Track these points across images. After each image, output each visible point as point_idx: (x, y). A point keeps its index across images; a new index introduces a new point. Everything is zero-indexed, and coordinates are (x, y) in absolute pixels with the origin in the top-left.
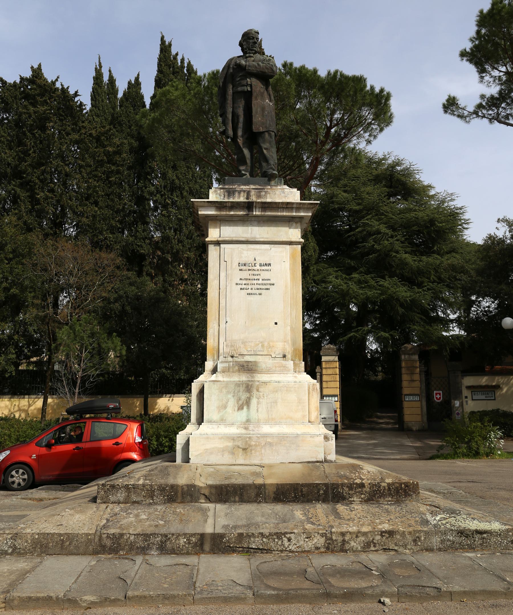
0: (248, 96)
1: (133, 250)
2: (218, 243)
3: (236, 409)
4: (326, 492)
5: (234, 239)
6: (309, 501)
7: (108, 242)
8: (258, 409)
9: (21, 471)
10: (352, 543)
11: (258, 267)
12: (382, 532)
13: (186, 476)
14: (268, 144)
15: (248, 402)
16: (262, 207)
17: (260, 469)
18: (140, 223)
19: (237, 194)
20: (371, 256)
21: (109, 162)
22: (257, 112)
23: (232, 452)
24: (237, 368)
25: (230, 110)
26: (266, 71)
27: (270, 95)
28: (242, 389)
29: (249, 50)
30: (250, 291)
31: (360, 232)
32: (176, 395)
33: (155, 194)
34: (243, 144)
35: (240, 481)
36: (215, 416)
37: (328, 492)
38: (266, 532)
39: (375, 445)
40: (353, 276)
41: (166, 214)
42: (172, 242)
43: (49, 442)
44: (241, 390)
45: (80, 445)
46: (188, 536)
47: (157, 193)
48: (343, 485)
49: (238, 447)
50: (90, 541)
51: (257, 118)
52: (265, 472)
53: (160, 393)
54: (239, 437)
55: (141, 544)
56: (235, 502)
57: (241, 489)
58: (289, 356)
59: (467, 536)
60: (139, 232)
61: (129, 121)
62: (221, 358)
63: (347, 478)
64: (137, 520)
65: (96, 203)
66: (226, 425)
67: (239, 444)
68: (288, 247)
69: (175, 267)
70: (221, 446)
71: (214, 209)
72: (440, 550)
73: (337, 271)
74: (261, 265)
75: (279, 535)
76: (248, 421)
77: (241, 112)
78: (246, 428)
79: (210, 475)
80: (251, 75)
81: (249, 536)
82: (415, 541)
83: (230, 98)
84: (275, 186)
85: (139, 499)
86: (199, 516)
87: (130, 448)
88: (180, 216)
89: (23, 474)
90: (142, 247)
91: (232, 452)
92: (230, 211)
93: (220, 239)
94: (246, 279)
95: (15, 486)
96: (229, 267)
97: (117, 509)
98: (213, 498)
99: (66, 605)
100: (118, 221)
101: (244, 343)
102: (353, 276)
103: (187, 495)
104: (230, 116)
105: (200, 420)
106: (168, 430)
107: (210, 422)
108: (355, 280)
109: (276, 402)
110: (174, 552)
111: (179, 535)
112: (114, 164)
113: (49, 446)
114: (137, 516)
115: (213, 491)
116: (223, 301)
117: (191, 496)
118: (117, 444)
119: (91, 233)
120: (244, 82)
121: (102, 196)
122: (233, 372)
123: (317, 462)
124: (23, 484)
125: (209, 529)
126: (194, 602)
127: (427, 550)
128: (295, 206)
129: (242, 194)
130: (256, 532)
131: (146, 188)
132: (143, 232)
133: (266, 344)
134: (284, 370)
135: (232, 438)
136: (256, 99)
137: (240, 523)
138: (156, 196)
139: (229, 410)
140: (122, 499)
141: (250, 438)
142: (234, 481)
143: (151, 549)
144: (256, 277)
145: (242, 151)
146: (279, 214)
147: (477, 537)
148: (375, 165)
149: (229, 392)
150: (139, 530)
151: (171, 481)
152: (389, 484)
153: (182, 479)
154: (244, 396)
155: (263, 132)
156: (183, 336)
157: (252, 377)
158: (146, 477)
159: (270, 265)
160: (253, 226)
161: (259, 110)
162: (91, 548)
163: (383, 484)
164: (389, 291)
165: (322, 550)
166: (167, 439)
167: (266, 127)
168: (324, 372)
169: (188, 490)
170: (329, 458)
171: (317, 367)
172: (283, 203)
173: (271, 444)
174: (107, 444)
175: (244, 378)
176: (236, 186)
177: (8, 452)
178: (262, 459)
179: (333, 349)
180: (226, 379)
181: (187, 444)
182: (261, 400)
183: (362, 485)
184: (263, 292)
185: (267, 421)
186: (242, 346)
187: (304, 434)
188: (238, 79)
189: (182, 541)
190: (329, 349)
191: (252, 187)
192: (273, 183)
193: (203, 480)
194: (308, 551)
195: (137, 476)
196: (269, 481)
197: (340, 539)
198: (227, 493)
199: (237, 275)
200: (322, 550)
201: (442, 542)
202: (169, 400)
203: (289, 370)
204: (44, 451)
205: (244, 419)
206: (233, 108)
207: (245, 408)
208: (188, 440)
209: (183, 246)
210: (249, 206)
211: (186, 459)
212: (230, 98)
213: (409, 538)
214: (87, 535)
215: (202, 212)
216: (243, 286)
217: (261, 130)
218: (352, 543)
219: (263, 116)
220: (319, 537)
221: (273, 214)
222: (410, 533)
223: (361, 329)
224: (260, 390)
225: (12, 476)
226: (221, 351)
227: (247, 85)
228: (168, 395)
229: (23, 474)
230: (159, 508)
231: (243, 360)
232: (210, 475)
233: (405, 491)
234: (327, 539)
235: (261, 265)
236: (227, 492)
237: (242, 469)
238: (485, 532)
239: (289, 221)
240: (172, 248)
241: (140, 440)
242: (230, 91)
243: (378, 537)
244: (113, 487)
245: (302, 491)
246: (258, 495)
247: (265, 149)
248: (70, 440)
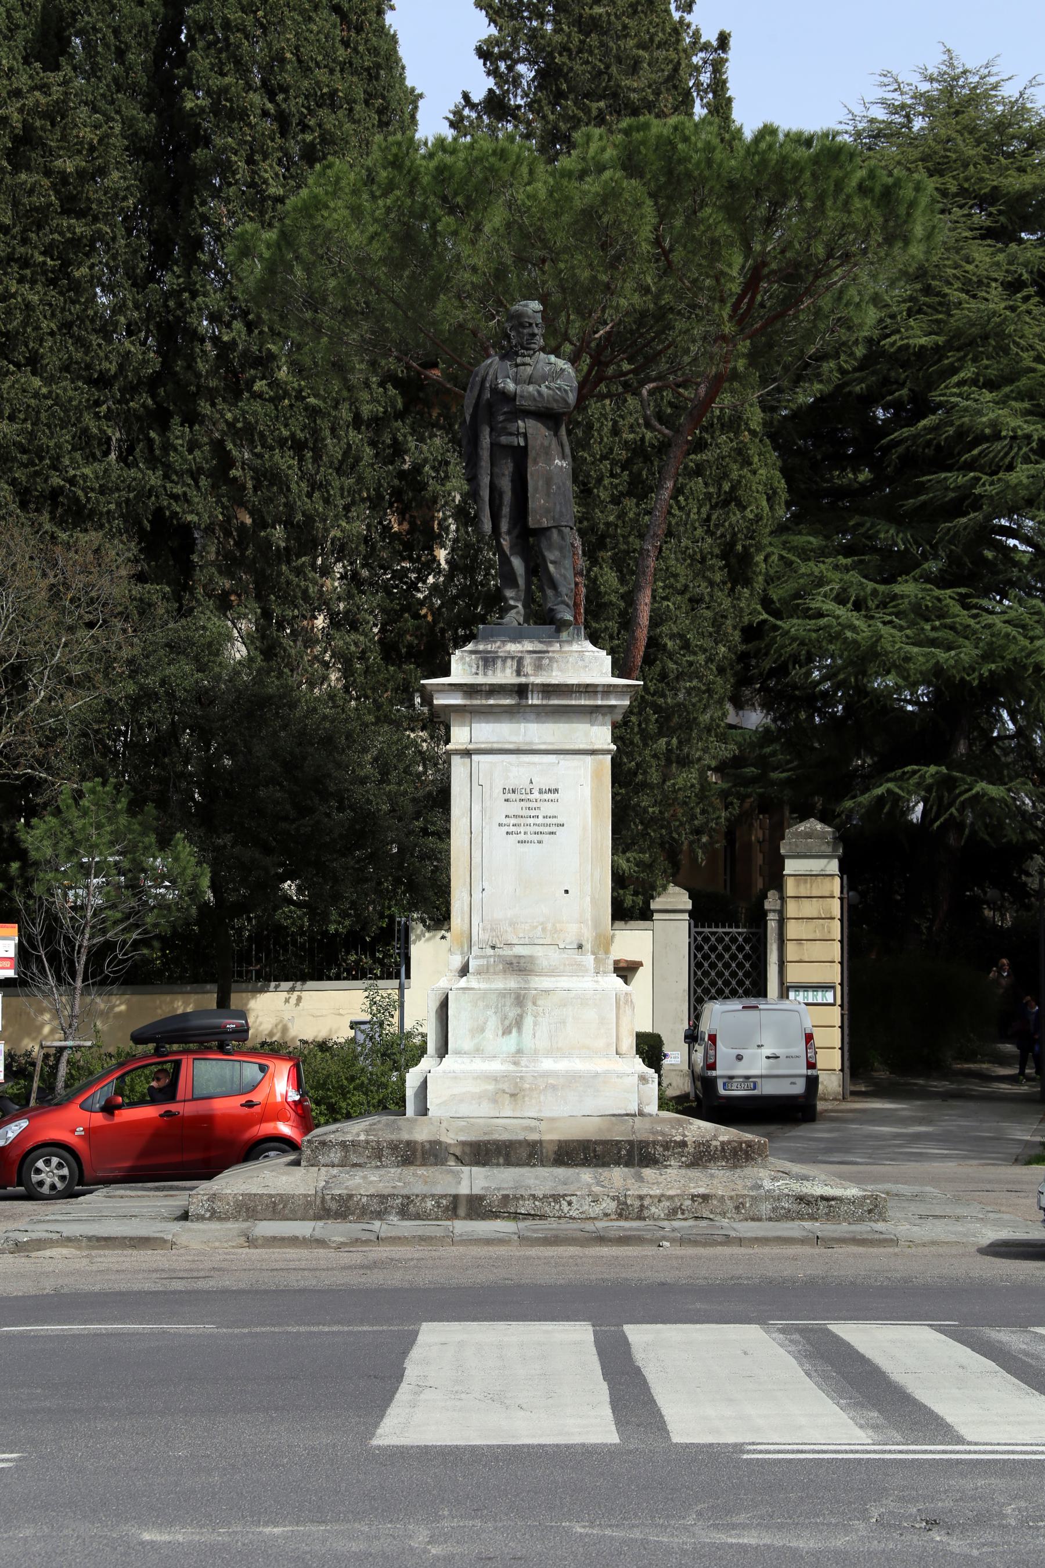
0: (520, 456)
1: (159, 510)
2: (467, 753)
3: (500, 1033)
4: (630, 1153)
5: (496, 746)
6: (605, 1165)
7: (80, 493)
8: (535, 1032)
9: (55, 1160)
10: (653, 1209)
11: (536, 795)
12: (693, 1196)
13: (426, 1131)
14: (557, 553)
15: (519, 1023)
16: (543, 692)
17: (533, 1123)
18: (177, 419)
19: (499, 663)
20: (964, 520)
21: (66, 212)
22: (536, 490)
23: (494, 1099)
24: (501, 967)
25: (485, 480)
26: (555, 406)
27: (562, 446)
28: (509, 1001)
29: (523, 348)
30: (522, 837)
31: (935, 429)
32: (310, 984)
33: (227, 318)
34: (511, 548)
35: (505, 1136)
36: (467, 1045)
37: (639, 1154)
38: (540, 1193)
39: (917, 1138)
40: (897, 589)
41: (265, 389)
42: (289, 489)
43: (108, 1101)
44: (508, 1004)
45: (173, 1107)
46: (438, 1198)
47: (234, 317)
48: (654, 1143)
49: (504, 1091)
50: (309, 1204)
51: (537, 501)
52: (543, 1126)
53: (258, 979)
54: (505, 1077)
55: (375, 1207)
56: (498, 1165)
57: (507, 1147)
58: (588, 946)
59: (809, 1203)
60: (176, 450)
61: (116, 32)
62: (474, 949)
63: (663, 1134)
64: (367, 1182)
65: (34, 362)
66: (485, 1058)
67: (505, 1086)
68: (589, 759)
69: (299, 572)
70: (477, 1090)
71: (460, 695)
72: (770, 1219)
73: (847, 569)
74: (541, 792)
75: (556, 1198)
76: (519, 1051)
77: (506, 484)
78: (515, 1063)
79: (461, 1130)
80: (526, 414)
81: (516, 1198)
82: (737, 1208)
83: (485, 454)
84: (567, 642)
85: (361, 1161)
86: (449, 1178)
87: (275, 1113)
88: (312, 400)
89: (60, 1166)
90: (187, 501)
91: (494, 1099)
92: (487, 699)
93: (470, 747)
94: (515, 816)
95: (45, 1190)
96: (486, 796)
97: (335, 1171)
98: (467, 1159)
99: (314, 1245)
100: (108, 416)
101: (512, 924)
102: (897, 589)
103: (431, 1154)
104: (485, 494)
105: (443, 1050)
106: (325, 1083)
107: (458, 1053)
108: (905, 605)
109: (563, 1022)
110: (418, 1217)
111: (425, 1196)
112: (81, 214)
113: (109, 1108)
114: (365, 1178)
115: (468, 1150)
116: (476, 854)
117: (436, 1156)
118: (249, 1104)
119: (26, 466)
120: (512, 427)
121: (52, 334)
122: (495, 973)
123: (627, 1115)
124: (60, 1186)
125: (464, 1190)
126: (453, 1243)
127: (753, 1219)
128: (600, 689)
129: (509, 662)
130: (526, 1193)
131: (194, 295)
132: (190, 451)
133: (549, 926)
134: (578, 970)
135: (495, 1079)
136: (536, 462)
137: (505, 1186)
138: (229, 325)
139: (489, 1034)
140: (336, 1161)
141: (521, 1078)
142: (496, 1137)
143: (389, 1213)
144: (533, 813)
145: (510, 563)
146: (573, 702)
147: (822, 1204)
148: (1015, 146)
149: (487, 1007)
150: (371, 1191)
151: (405, 1136)
152: (723, 1143)
153: (421, 1133)
154: (512, 1013)
155: (548, 529)
156: (340, 809)
157: (527, 982)
158: (367, 1132)
159: (556, 791)
160: (527, 721)
161: (540, 483)
162: (311, 1212)
163: (714, 1143)
164: (1013, 647)
165: (613, 1217)
166: (323, 1107)
167: (554, 519)
168: (792, 909)
169: (431, 1148)
170: (647, 1110)
171: (770, 894)
172: (579, 685)
173: (554, 1088)
174: (228, 1106)
175: (512, 983)
176: (498, 644)
177: (24, 1123)
178: (540, 1111)
179: (822, 836)
180: (483, 986)
181: (424, 1084)
182: (540, 1019)
183: (683, 1144)
184: (545, 838)
185: (550, 1053)
186: (509, 929)
187: (607, 1072)
188: (501, 418)
189: (430, 1204)
190: (809, 835)
191: (528, 646)
192: (564, 635)
193: (451, 1135)
194: (595, 1218)
195: (354, 1132)
196: (546, 1137)
197: (637, 1203)
198: (483, 1152)
199: (501, 810)
200: (613, 1217)
201: (774, 1210)
202: (287, 1001)
203: (587, 971)
204: (99, 1119)
205: (513, 1049)
206: (492, 475)
207: (514, 1031)
208: (425, 1081)
209: (327, 501)
210: (521, 690)
211: (424, 1111)
212: (485, 454)
213: (730, 1205)
214: (306, 1196)
215: (439, 701)
216: (512, 829)
217: (545, 523)
218: (653, 1209)
219: (548, 494)
220: (608, 1200)
221: (563, 702)
222: (731, 1198)
223: (914, 772)
224: (539, 1002)
225: (38, 1171)
226: (475, 938)
227: (518, 434)
228: (286, 985)
229: (60, 1166)
230: (393, 1170)
231: (510, 953)
232: (462, 1130)
233: (746, 1153)
234: (619, 1203)
235: (541, 792)
236: (487, 1151)
237: (509, 1122)
238: (833, 1199)
239: (591, 713)
240: (290, 507)
241: (297, 1098)
242: (486, 441)
243: (688, 1202)
244: (323, 1143)
245: (595, 1151)
246: (531, 1156)
247: (552, 562)
248: (154, 1097)
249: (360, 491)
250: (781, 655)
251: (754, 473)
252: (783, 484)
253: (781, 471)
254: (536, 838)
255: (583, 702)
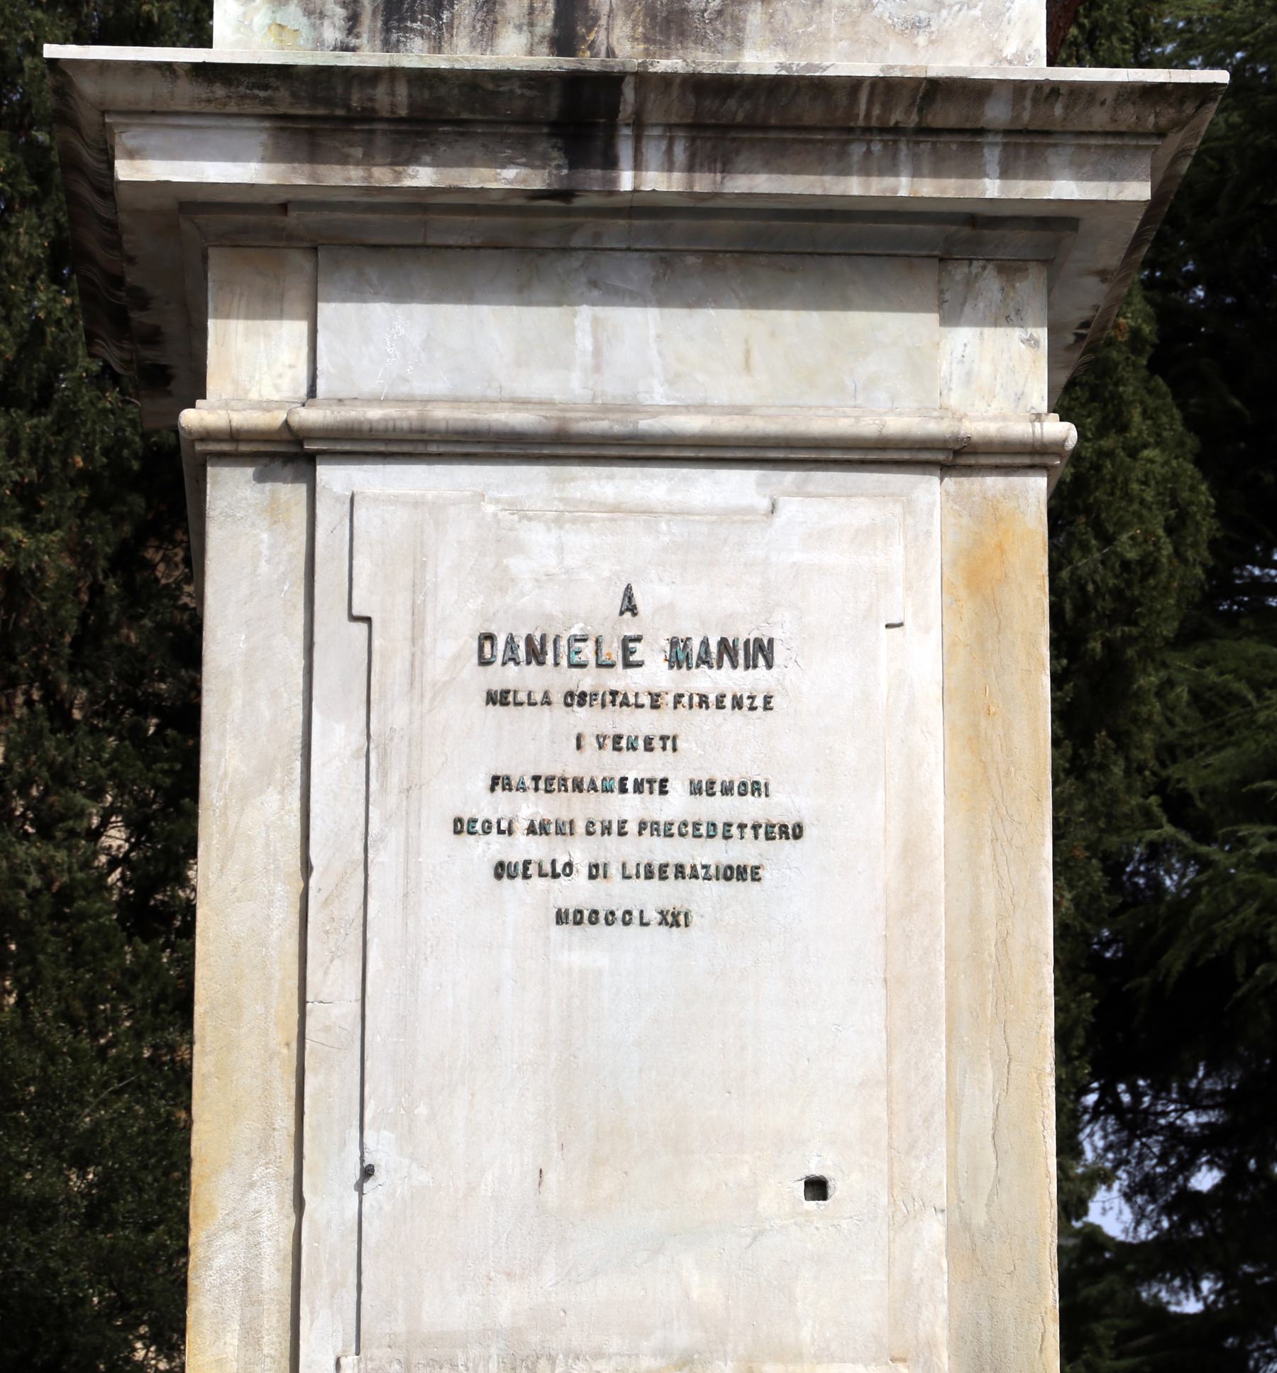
2: (290, 453)
11: (654, 673)
30: (577, 891)
68: (929, 490)
71: (257, 136)
74: (678, 655)
92: (404, 156)
94: (546, 784)
96: (392, 672)
116: (333, 983)
128: (996, 113)
144: (637, 766)
146: (854, 186)
159: (761, 652)
184: (702, 897)
199: (465, 748)
216: (523, 848)
235: (678, 655)
239: (942, 257)
249: (67, 451)
250: (1212, 937)
251: (1133, 453)
252: (1204, 494)
253: (1198, 461)
254: (653, 896)
255: (903, 186)
